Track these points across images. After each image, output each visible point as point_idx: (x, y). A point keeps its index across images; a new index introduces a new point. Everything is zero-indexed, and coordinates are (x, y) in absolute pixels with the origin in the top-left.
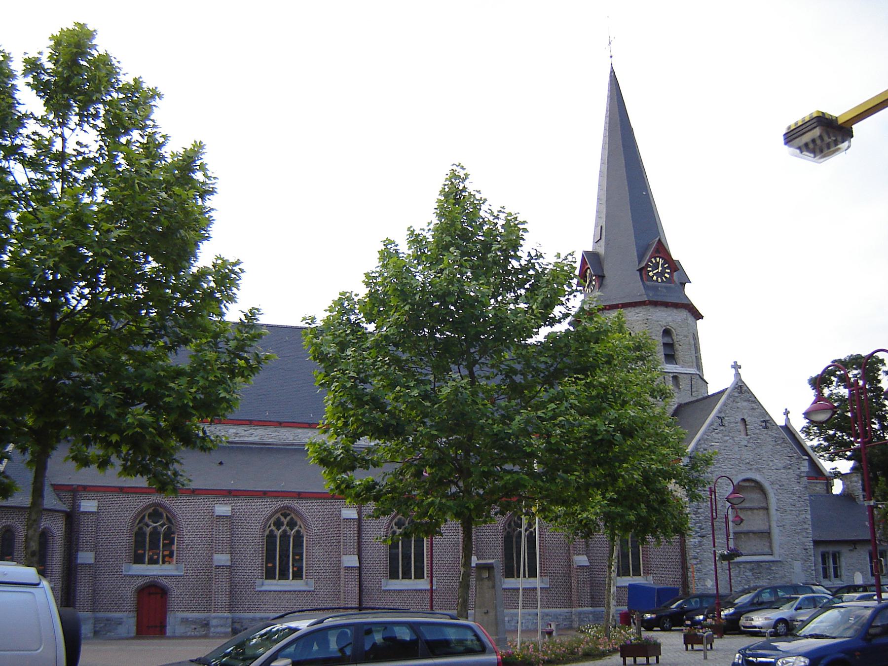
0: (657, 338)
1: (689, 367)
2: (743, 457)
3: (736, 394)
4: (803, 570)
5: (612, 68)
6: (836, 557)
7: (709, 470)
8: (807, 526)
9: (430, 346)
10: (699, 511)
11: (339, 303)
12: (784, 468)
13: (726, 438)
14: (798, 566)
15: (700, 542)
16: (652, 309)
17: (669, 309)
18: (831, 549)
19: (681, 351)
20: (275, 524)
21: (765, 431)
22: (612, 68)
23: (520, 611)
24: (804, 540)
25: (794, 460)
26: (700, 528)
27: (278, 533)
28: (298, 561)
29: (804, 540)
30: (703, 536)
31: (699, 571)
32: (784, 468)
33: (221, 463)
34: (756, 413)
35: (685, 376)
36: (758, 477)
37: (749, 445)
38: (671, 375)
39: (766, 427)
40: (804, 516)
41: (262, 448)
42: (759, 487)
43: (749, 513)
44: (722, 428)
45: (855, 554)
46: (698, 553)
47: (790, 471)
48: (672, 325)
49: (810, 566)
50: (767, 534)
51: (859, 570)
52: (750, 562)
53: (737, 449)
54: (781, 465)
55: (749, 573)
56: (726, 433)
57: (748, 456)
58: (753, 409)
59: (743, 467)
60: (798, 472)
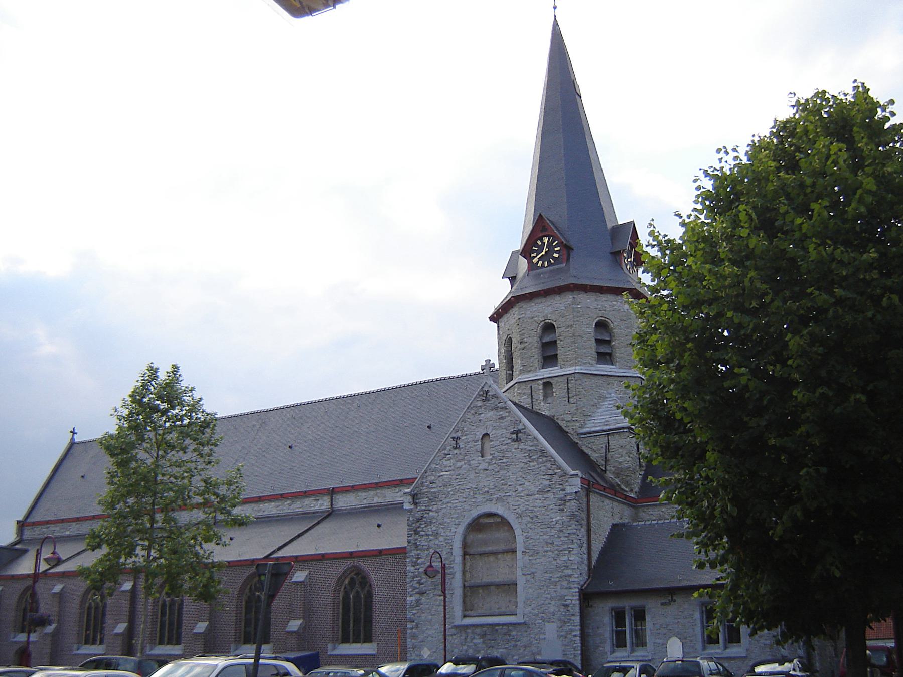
0: (530, 340)
1: (571, 365)
2: (481, 485)
3: (479, 404)
4: (559, 637)
5: (556, 23)
6: (640, 615)
8: (570, 572)
9: (181, 420)
10: (419, 561)
11: (137, 397)
12: (541, 492)
13: (459, 464)
14: (551, 630)
16: (524, 305)
17: (549, 298)
18: (627, 604)
21: (516, 445)
22: (556, 23)
24: (565, 592)
25: (556, 477)
26: (420, 583)
29: (565, 592)
30: (422, 593)
31: (414, 637)
32: (541, 492)
34: (505, 423)
36: (499, 509)
37: (490, 468)
39: (518, 440)
40: (566, 558)
42: (504, 523)
43: (492, 558)
44: (456, 451)
45: (672, 610)
46: (414, 614)
47: (550, 495)
48: (552, 319)
49: (572, 630)
50: (510, 587)
51: (677, 635)
52: (482, 626)
53: (472, 475)
54: (534, 489)
55: (478, 641)
56: (460, 457)
57: (487, 482)
58: (502, 418)
59: (480, 498)
60: (561, 495)
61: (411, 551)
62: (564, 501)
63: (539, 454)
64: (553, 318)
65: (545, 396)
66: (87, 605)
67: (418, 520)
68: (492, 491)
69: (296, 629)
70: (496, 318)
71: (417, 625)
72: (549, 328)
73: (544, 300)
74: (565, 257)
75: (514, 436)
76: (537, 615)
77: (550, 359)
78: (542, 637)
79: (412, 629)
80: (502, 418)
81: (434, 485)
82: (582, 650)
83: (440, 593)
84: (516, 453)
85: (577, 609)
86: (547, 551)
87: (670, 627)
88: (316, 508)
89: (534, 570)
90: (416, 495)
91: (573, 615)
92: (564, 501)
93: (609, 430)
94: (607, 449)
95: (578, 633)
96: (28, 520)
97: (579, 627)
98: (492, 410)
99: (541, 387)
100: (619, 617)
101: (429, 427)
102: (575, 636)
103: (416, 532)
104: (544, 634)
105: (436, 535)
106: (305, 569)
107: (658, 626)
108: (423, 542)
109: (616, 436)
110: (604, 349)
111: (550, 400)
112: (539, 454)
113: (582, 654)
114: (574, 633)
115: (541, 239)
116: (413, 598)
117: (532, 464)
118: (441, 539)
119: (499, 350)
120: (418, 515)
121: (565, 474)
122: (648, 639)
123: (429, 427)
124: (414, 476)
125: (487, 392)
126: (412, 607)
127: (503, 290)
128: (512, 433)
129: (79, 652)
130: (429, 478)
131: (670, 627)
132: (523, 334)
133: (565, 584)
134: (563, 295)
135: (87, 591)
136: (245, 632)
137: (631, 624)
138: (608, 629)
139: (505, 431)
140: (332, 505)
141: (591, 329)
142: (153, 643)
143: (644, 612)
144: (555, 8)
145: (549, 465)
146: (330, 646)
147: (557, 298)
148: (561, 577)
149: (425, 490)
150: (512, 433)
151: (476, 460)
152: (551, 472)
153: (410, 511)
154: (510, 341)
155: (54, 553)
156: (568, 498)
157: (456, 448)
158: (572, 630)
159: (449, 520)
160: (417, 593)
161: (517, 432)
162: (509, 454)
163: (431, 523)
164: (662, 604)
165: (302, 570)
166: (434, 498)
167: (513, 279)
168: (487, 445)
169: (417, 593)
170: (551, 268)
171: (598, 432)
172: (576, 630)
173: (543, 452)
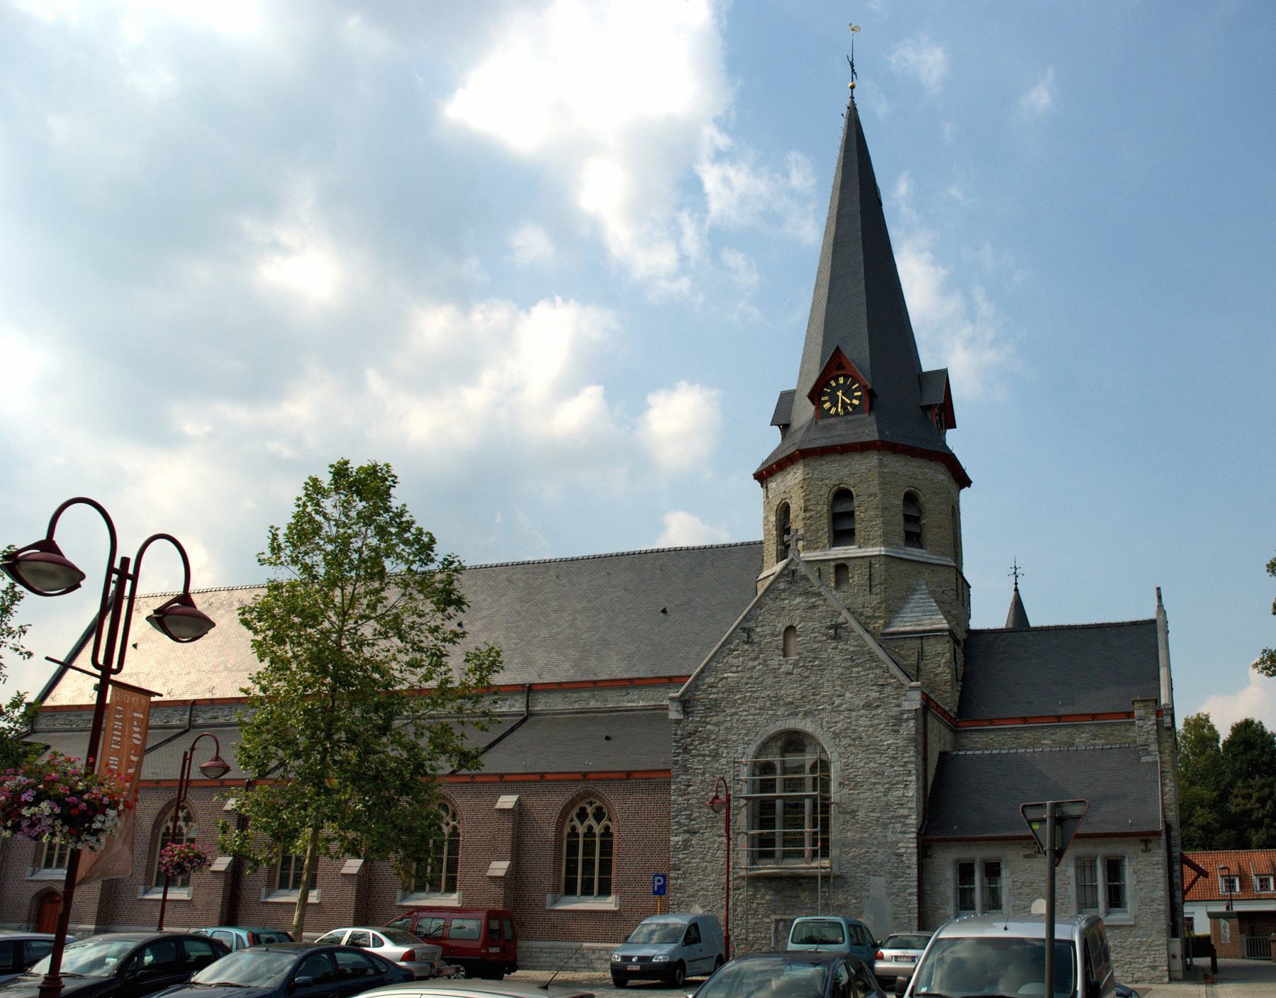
1: (873, 545)
5: (853, 110)
6: (993, 870)
7: (715, 720)
12: (867, 706)
13: (751, 664)
15: (685, 841)
19: (931, 525)
20: (578, 816)
22: (853, 110)
23: (915, 933)
25: (888, 690)
26: (689, 817)
27: (581, 830)
28: (606, 867)
32: (867, 706)
33: (608, 738)
34: (817, 614)
35: (858, 562)
38: (833, 564)
39: (836, 637)
41: (595, 718)
48: (850, 484)
53: (770, 681)
54: (859, 702)
57: (791, 691)
61: (678, 776)
62: (899, 720)
63: (867, 657)
64: (851, 481)
65: (838, 583)
66: (163, 830)
67: (690, 735)
68: (798, 703)
69: (502, 873)
70: (763, 476)
71: (684, 873)
72: (843, 495)
73: (839, 458)
74: (867, 404)
75: (832, 631)
76: (858, 866)
77: (842, 535)
78: (864, 893)
79: (677, 879)
80: (814, 607)
81: (714, 690)
82: (919, 913)
83: (723, 831)
84: (832, 651)
85: (914, 859)
86: (875, 784)
87: (1035, 886)
88: (504, 709)
89: (855, 808)
90: (688, 701)
91: (909, 867)
92: (899, 720)
93: (924, 631)
94: (921, 656)
95: (915, 890)
96: (48, 702)
97: (915, 883)
98: (800, 595)
99: (832, 570)
100: (965, 872)
101: (664, 611)
102: (910, 894)
103: (686, 751)
104: (868, 890)
105: (716, 755)
106: (514, 793)
107: (1019, 884)
108: (695, 764)
109: (932, 641)
110: (914, 529)
111: (844, 588)
112: (867, 657)
113: (919, 918)
114: (909, 891)
115: (836, 380)
116: (679, 838)
117: (855, 670)
118: (723, 761)
119: (766, 518)
120: (690, 727)
121: (901, 686)
122: (1004, 899)
123: (664, 611)
124: (684, 672)
125: (794, 572)
126: (677, 850)
127: (770, 442)
128: (830, 628)
129: (270, 900)
130: (707, 680)
131: (1035, 886)
132: (808, 500)
133: (898, 826)
134: (865, 454)
135: (163, 813)
136: (567, 879)
137: (982, 882)
138: (952, 884)
139: (817, 625)
140: (528, 706)
141: (899, 502)
142: (407, 891)
143: (998, 865)
144: (852, 87)
145: (878, 671)
146: (549, 897)
147: (857, 457)
148: (893, 817)
149: (699, 695)
150: (830, 628)
151: (776, 660)
152: (881, 682)
153: (678, 722)
154: (784, 510)
155: (217, 758)
156: (905, 716)
157: (747, 643)
158: (906, 887)
159: (735, 738)
160: (685, 832)
161: (836, 627)
162: (824, 655)
163: (708, 739)
164: (1026, 856)
165: (509, 793)
166: (714, 706)
167: (785, 428)
168: (793, 642)
169: (685, 832)
170: (849, 418)
171: (910, 632)
172: (911, 887)
173: (872, 657)
